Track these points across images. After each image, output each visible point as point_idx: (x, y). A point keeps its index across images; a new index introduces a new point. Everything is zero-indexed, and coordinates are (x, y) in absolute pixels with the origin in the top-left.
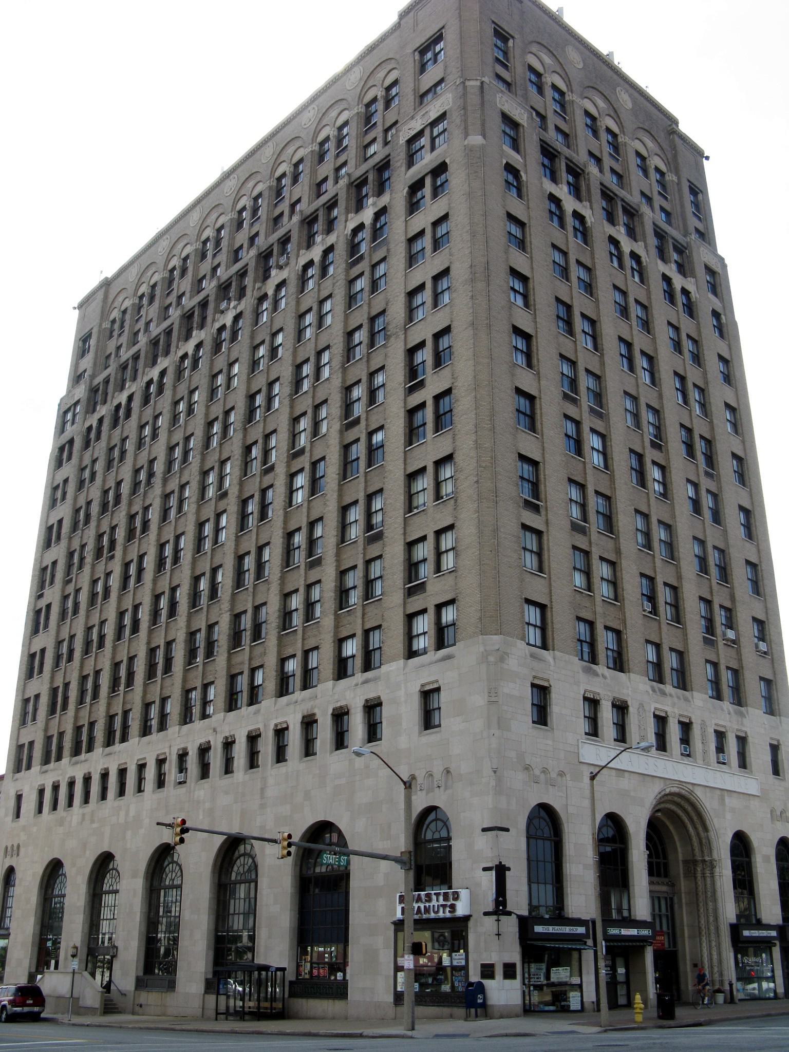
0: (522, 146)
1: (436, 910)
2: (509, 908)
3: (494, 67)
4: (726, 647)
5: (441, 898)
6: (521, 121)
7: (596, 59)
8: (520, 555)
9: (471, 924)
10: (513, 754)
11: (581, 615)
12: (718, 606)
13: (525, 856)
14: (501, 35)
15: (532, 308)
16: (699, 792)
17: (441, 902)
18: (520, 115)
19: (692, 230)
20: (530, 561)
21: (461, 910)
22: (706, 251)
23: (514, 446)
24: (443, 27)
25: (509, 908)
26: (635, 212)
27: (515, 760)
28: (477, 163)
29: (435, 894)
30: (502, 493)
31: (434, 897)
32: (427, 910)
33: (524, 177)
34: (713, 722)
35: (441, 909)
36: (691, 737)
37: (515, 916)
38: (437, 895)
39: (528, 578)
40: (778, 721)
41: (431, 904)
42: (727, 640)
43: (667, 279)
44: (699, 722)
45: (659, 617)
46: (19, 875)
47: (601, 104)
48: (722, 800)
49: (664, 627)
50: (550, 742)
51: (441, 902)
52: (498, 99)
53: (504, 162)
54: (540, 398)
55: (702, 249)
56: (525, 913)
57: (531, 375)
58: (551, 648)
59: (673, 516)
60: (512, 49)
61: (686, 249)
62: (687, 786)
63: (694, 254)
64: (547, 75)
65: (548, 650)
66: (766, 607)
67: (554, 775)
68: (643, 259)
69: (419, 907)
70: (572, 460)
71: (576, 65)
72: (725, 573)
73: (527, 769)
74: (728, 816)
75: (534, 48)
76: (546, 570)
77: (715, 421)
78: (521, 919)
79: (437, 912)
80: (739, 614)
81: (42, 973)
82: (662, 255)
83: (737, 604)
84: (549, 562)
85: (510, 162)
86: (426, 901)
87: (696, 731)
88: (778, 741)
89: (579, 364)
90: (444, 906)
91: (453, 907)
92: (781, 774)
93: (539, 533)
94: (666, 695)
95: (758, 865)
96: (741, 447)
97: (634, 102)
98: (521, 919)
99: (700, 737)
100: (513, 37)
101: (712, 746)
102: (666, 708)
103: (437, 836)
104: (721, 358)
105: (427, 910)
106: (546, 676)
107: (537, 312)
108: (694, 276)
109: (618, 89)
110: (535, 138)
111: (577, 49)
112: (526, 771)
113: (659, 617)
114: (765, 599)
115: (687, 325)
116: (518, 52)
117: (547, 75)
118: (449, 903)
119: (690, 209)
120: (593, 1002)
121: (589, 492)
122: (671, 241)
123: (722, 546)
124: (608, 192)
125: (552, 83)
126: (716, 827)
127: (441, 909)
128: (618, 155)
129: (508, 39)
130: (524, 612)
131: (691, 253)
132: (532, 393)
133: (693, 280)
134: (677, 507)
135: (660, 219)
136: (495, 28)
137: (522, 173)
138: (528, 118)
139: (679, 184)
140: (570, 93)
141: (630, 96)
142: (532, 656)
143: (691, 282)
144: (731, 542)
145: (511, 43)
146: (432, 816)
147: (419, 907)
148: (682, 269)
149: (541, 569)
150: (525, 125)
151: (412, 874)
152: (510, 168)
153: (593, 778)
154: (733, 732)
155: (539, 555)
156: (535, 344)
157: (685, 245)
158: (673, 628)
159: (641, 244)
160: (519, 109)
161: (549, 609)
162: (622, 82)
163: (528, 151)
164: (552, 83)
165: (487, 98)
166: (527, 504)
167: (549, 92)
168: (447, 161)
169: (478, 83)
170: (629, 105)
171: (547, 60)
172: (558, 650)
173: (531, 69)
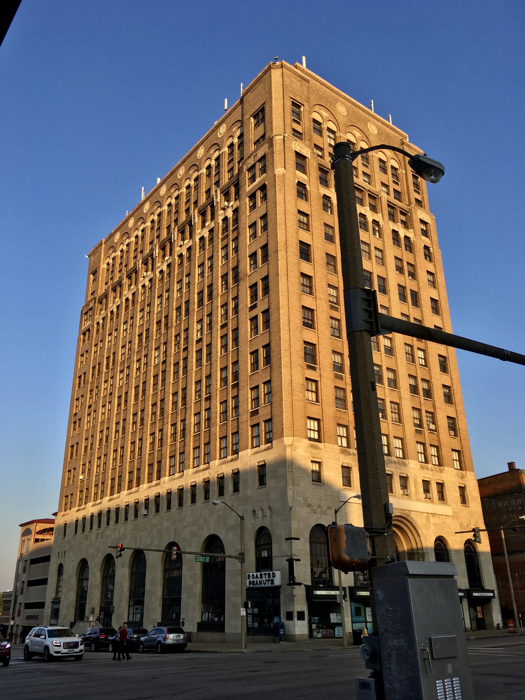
0: (308, 170)
1: (265, 582)
2: (297, 581)
3: (291, 125)
4: (430, 433)
5: (267, 576)
6: (307, 156)
7: (355, 108)
8: (305, 394)
9: (281, 590)
10: (301, 499)
11: (340, 423)
12: (425, 412)
13: (309, 553)
14: (296, 105)
15: (313, 261)
16: (413, 515)
17: (267, 578)
18: (306, 152)
19: (413, 201)
20: (312, 396)
21: (277, 581)
22: (421, 212)
23: (302, 337)
24: (264, 103)
25: (297, 581)
26: (376, 197)
27: (303, 502)
28: (281, 184)
29: (264, 574)
30: (294, 363)
31: (264, 576)
32: (260, 582)
33: (308, 189)
34: (422, 476)
35: (267, 582)
36: (408, 485)
37: (304, 586)
38: (265, 574)
39: (309, 406)
40: (465, 474)
41: (262, 579)
42: (431, 430)
43: (395, 233)
44: (413, 476)
45: (387, 420)
46: (65, 568)
47: (358, 134)
48: (428, 519)
49: (391, 426)
50: (322, 491)
51: (267, 578)
52: (293, 145)
53: (297, 181)
54: (316, 310)
55: (418, 211)
56: (310, 584)
57: (311, 298)
58: (323, 441)
59: (397, 365)
60: (303, 113)
61: (408, 212)
62: (405, 511)
63: (414, 215)
64: (324, 124)
65: (321, 443)
66: (456, 410)
67: (325, 509)
68: (381, 224)
69: (257, 581)
70: (335, 341)
71: (343, 114)
72: (428, 393)
73: (309, 506)
74: (432, 528)
75: (317, 108)
76: (320, 401)
77: (424, 310)
78: (307, 587)
79: (265, 584)
80: (437, 415)
81: (295, 450)
82: (392, 217)
83: (437, 410)
84: (321, 397)
85: (300, 181)
86: (260, 577)
87: (411, 482)
88: (465, 485)
89: (340, 288)
90: (268, 580)
91: (272, 581)
92: (467, 503)
93: (316, 381)
94: (392, 462)
95: (452, 555)
96: (441, 322)
97: (379, 129)
98: (307, 587)
99: (414, 485)
100: (303, 105)
101: (421, 489)
102: (392, 470)
103: (266, 542)
104: (429, 272)
105: (260, 582)
106: (320, 457)
107: (315, 263)
108: (413, 228)
109: (369, 123)
110: (315, 164)
111: (344, 104)
112: (309, 507)
113: (387, 420)
114: (456, 406)
115: (407, 257)
116: (306, 114)
117: (324, 124)
118: (270, 579)
119: (412, 188)
120: (350, 633)
121: (345, 357)
122: (399, 209)
123: (427, 378)
124: (360, 188)
125: (328, 127)
126: (425, 534)
127: (267, 582)
128: (368, 163)
129: (301, 106)
130: (307, 424)
131: (411, 214)
132: (312, 308)
133: (412, 230)
134: (398, 360)
135: (392, 198)
136: (292, 102)
137: (307, 186)
138: (311, 153)
139: (406, 174)
140: (339, 132)
141: (377, 126)
142: (312, 446)
143: (411, 232)
144: (433, 376)
145: (302, 108)
146: (264, 532)
147: (257, 581)
148: (406, 225)
149: (317, 401)
150: (309, 157)
151: (449, 548)
152: (301, 185)
153: (336, 512)
154: (434, 481)
155: (316, 392)
156: (314, 281)
157: (408, 211)
158: (396, 425)
159: (380, 215)
160: (306, 148)
161: (322, 421)
162: (371, 118)
163: (311, 172)
164: (328, 127)
165: (286, 145)
166: (309, 367)
167: (326, 133)
168: (266, 183)
169: (282, 137)
170: (376, 132)
171: (325, 114)
172: (327, 443)
173: (315, 121)
